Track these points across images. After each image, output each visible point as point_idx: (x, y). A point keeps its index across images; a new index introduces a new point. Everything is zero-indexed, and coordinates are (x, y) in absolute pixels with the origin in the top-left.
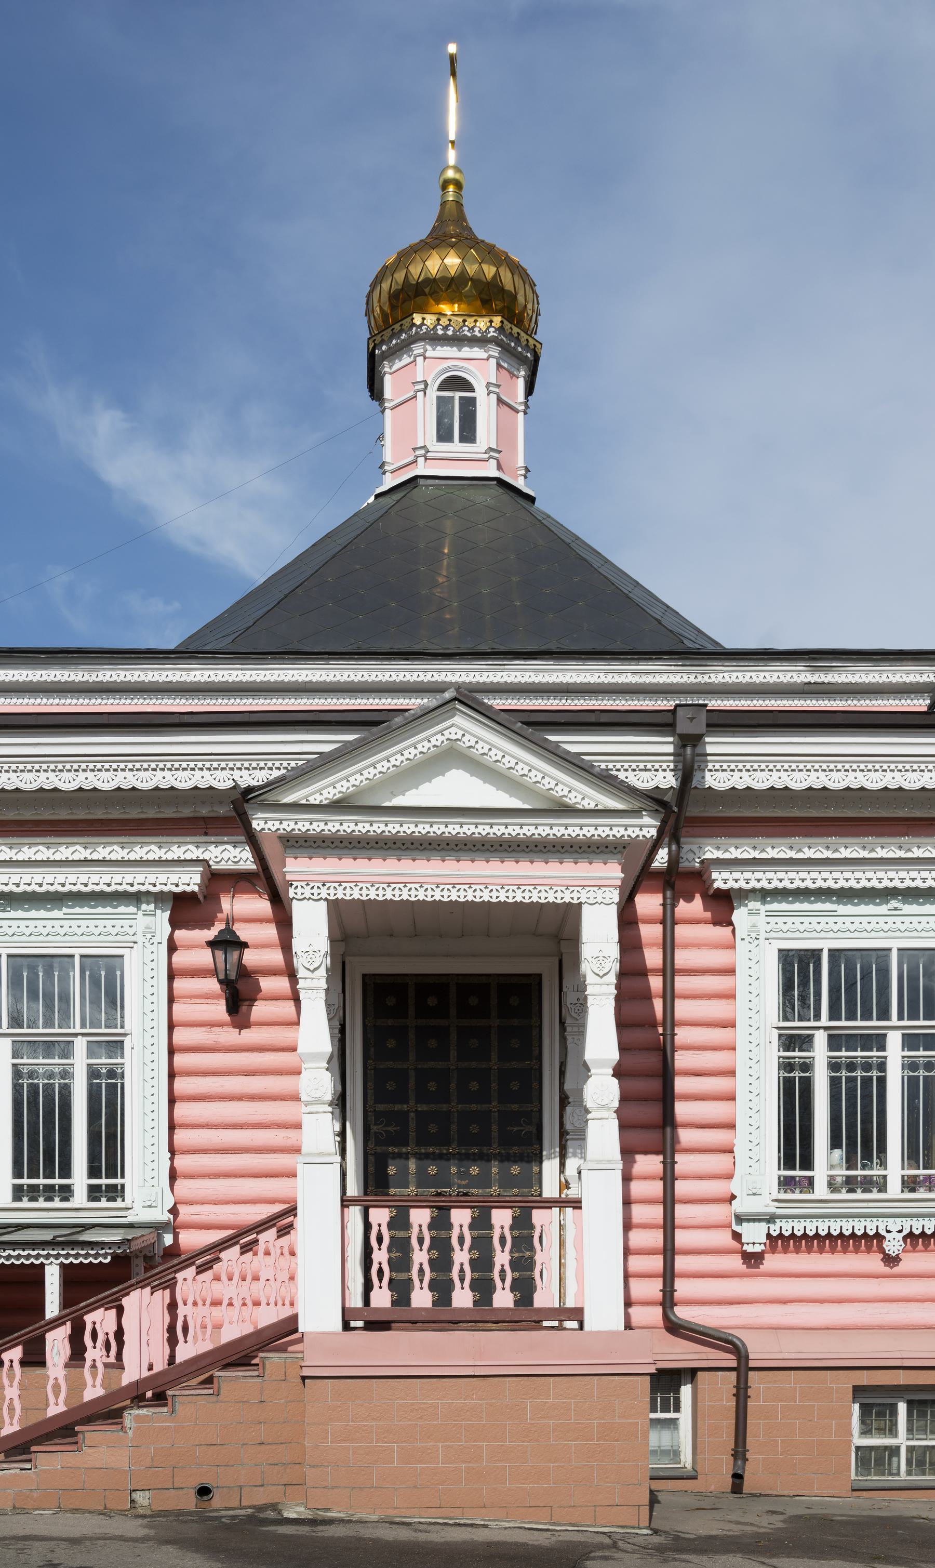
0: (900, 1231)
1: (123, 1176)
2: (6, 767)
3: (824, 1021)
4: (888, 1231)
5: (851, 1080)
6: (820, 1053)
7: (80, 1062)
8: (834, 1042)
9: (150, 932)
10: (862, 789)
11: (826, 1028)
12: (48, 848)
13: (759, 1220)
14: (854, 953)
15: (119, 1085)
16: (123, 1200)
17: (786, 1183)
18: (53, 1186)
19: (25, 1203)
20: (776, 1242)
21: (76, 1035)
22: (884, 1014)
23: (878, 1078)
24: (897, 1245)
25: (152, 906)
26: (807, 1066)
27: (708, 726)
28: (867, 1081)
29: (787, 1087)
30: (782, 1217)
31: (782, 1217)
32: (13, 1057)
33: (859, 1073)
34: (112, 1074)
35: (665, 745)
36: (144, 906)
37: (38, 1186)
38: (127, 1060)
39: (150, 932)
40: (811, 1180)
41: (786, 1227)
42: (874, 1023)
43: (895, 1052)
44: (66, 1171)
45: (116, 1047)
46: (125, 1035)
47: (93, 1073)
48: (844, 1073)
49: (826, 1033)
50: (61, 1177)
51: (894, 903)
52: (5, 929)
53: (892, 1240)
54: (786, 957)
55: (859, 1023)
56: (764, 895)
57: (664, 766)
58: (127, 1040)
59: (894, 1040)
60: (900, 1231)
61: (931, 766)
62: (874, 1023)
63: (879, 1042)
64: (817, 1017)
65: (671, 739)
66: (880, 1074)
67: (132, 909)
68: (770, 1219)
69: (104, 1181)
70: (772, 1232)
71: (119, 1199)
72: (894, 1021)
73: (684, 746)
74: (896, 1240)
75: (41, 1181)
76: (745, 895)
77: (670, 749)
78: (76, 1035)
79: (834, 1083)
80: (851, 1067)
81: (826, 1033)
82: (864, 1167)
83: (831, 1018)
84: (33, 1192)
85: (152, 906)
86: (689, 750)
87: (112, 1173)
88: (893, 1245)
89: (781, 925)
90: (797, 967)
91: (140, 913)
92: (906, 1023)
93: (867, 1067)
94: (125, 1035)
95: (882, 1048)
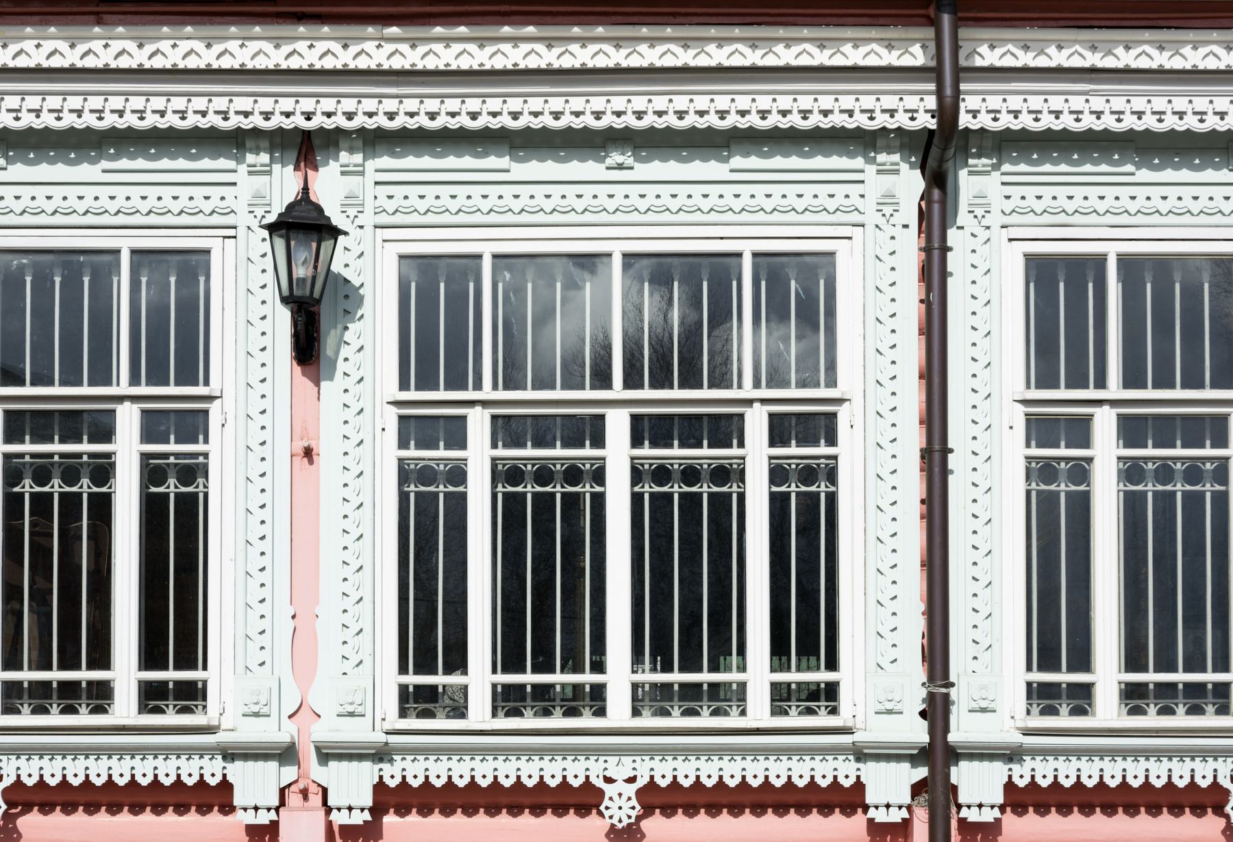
0: (631, 780)
1: (205, 668)
3: (1114, 388)
4: (609, 780)
5: (1165, 502)
6: (1106, 449)
7: (127, 448)
8: (1131, 431)
9: (888, 201)
11: (1113, 403)
12: (549, 47)
13: (360, 757)
14: (669, 260)
15: (201, 496)
17: (1043, 696)
18: (1173, 685)
20: (1020, 799)
21: (120, 399)
22: (102, 375)
23: (593, 495)
24: (626, 806)
26: (1081, 471)
28: (573, 503)
30: (1035, 752)
31: (1035, 752)
32: (772, 444)
33: (56, 487)
36: (250, 158)
37: (523, 686)
38: (213, 447)
39: (888, 201)
40: (598, 692)
41: (1044, 771)
42: (1062, 393)
43: (618, 452)
45: (192, 424)
47: (152, 471)
48: (823, 488)
52: (9, 202)
53: (616, 798)
54: (1042, 271)
55: (1178, 393)
58: (843, 414)
60: (631, 780)
63: (594, 431)
64: (1101, 383)
66: (1218, 488)
67: (859, 162)
68: (1012, 755)
70: (1016, 780)
71: (735, 711)
74: (624, 798)
90: (1060, 287)
91: (243, 169)
93: (1194, 472)
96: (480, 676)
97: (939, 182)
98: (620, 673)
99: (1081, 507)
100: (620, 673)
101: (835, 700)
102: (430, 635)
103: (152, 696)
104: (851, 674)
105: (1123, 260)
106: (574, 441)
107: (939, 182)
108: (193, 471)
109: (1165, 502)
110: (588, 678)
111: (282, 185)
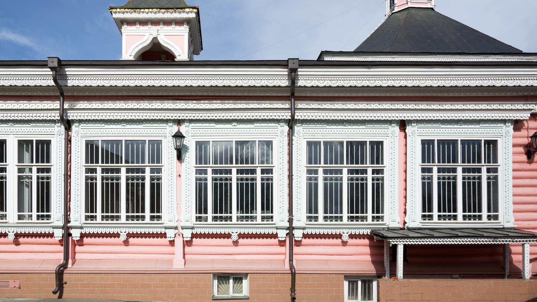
2: (2, 78)
3: (322, 164)
6: (99, 175)
7: (148, 175)
9: (282, 131)
10: (519, 86)
13: (300, 229)
16: (272, 221)
17: (309, 218)
18: (134, 216)
19: (467, 221)
20: (305, 236)
21: (146, 166)
22: (342, 163)
25: (60, 124)
27: (299, 65)
28: (226, 184)
30: (308, 228)
31: (308, 228)
33: (110, 181)
34: (429, 179)
35: (284, 72)
40: (231, 217)
41: (309, 231)
44: (455, 210)
45: (496, 170)
46: (51, 166)
47: (152, 179)
49: (101, 168)
50: (220, 213)
51: (234, 124)
54: (424, 142)
56: (191, 121)
57: (50, 78)
59: (459, 170)
61: (535, 78)
62: (203, 165)
65: (287, 70)
67: (502, 125)
68: (304, 228)
69: (156, 214)
72: (345, 165)
73: (291, 73)
76: (410, 122)
77: (287, 73)
78: (146, 166)
80: (331, 179)
81: (101, 168)
82: (251, 213)
83: (438, 163)
84: (470, 217)
85: (60, 124)
86: (293, 73)
87: (362, 212)
88: (345, 238)
89: (313, 132)
91: (168, 126)
92: (349, 165)
94: (51, 166)
95: (341, 173)
98: (123, 213)
99: (316, 185)
100: (123, 213)
102: (201, 207)
103: (152, 218)
107: (291, 128)
108: (496, 178)
110: (229, 215)
111: (175, 129)
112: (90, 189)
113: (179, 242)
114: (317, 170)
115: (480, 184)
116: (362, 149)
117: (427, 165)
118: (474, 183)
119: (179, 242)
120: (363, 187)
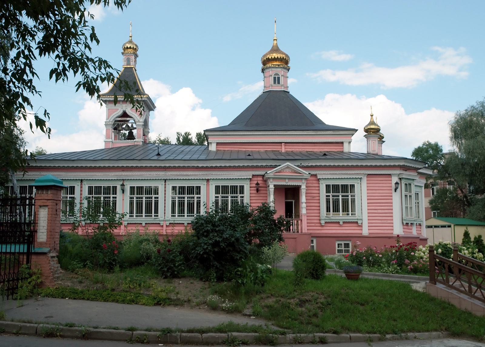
6: (135, 199)
7: (153, 199)
8: (146, 198)
17: (172, 216)
20: (326, 223)
29: (327, 201)
40: (133, 216)
45: (354, 196)
54: (326, 185)
63: (339, 196)
69: (156, 214)
75: (148, 214)
79: (145, 203)
87: (157, 213)
95: (133, 199)
96: (135, 214)
97: (165, 182)
101: (438, 216)
103: (352, 214)
104: (159, 214)
105: (332, 185)
106: (227, 198)
107: (165, 182)
109: (190, 202)
111: (121, 183)
112: (328, 201)
113: (165, 226)
114: (339, 196)
115: (151, 203)
116: (236, 188)
117: (217, 195)
118: (181, 203)
119: (165, 226)
120: (142, 203)
